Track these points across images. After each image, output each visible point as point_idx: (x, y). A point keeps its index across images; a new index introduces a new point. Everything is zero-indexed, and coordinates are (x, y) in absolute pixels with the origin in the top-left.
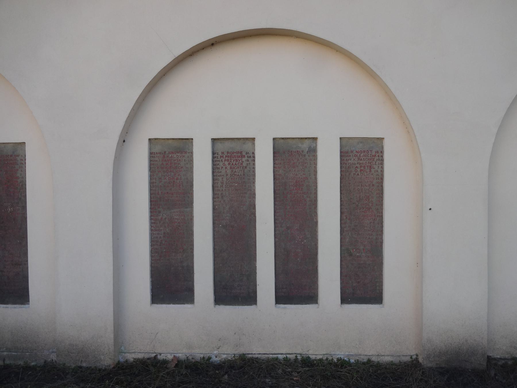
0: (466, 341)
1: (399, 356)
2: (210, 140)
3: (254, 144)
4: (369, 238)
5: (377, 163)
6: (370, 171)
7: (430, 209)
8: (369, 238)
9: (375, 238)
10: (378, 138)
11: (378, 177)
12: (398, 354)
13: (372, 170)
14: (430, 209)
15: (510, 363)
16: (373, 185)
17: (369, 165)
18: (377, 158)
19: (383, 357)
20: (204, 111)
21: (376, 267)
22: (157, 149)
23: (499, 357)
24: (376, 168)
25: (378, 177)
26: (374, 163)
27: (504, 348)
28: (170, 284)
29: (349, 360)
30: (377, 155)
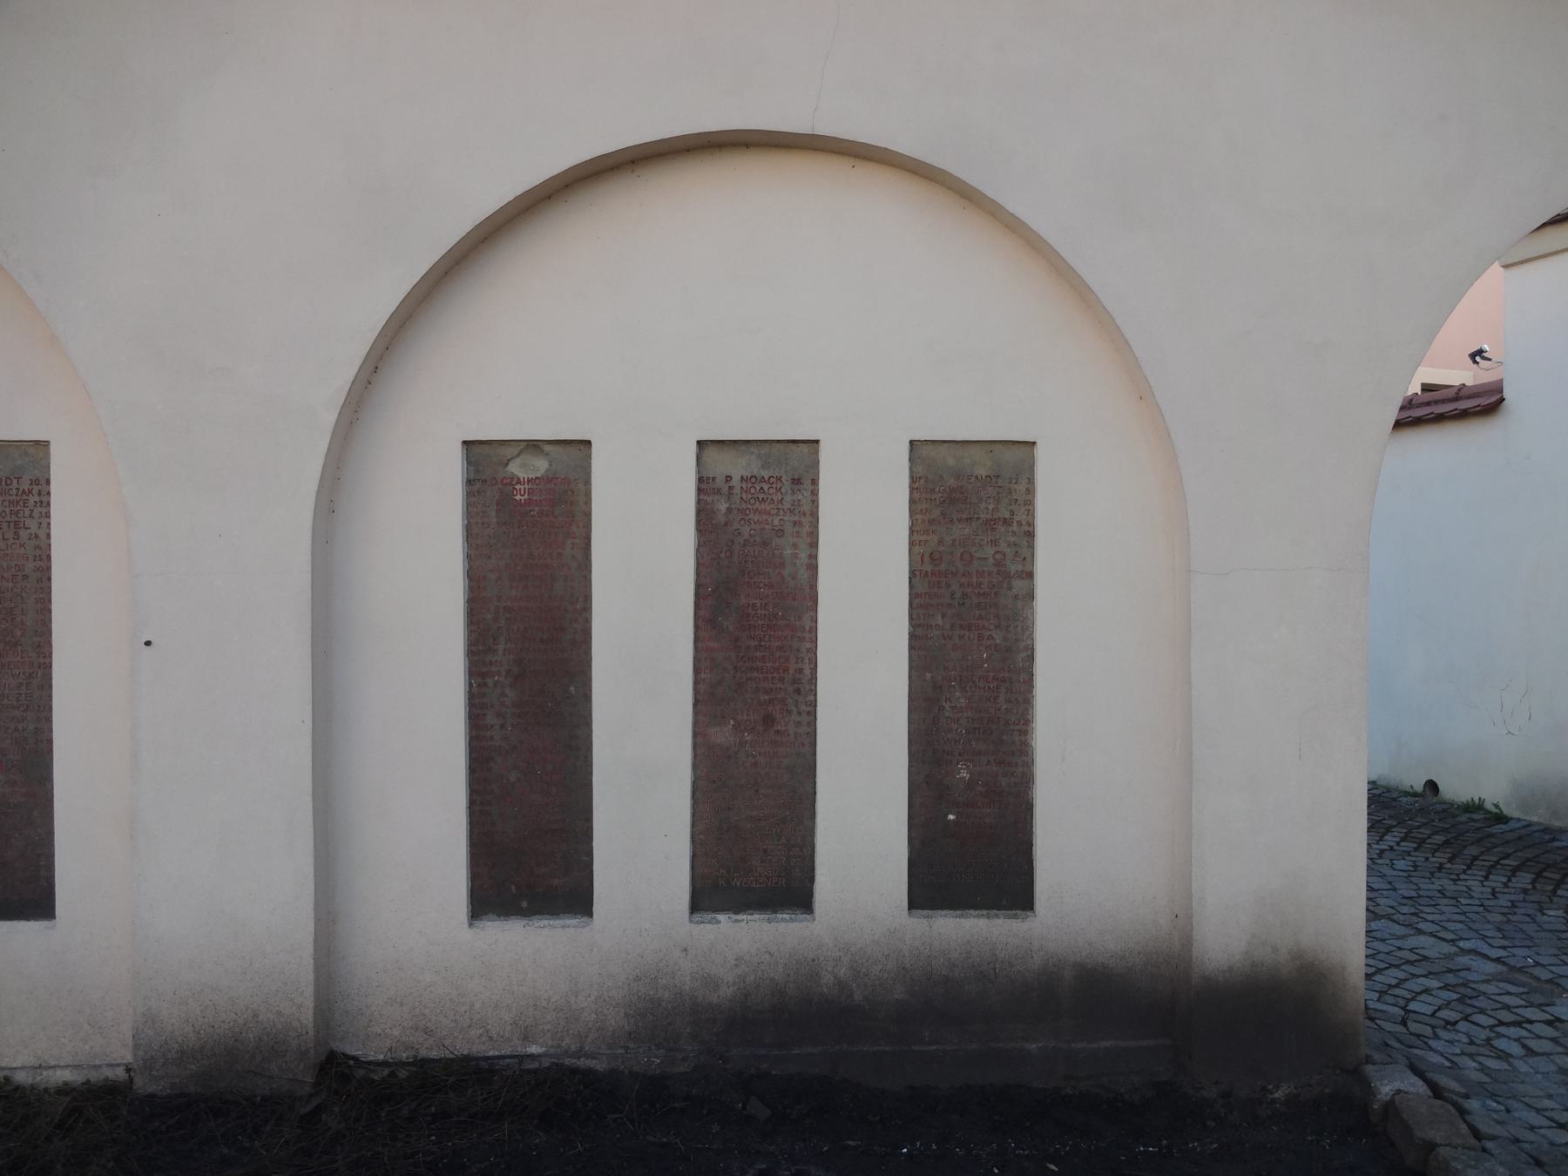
0: (256, 1016)
1: (97, 1067)
2: (460, 444)
3: (817, 452)
4: (16, 729)
5: (35, 514)
6: (17, 536)
7: (148, 643)
8: (16, 729)
9: (31, 727)
10: (37, 442)
11: (38, 552)
12: (98, 1062)
13: (22, 533)
14: (148, 643)
15: (402, 1074)
16: (25, 577)
17: (14, 518)
18: (37, 499)
19: (50, 1072)
20: (641, 364)
21: (35, 813)
22: (736, 467)
23: (381, 1057)
24: (34, 529)
25: (38, 552)
26: (27, 513)
27: (396, 1033)
28: (528, 849)
29: (131, 1080)
30: (35, 492)
